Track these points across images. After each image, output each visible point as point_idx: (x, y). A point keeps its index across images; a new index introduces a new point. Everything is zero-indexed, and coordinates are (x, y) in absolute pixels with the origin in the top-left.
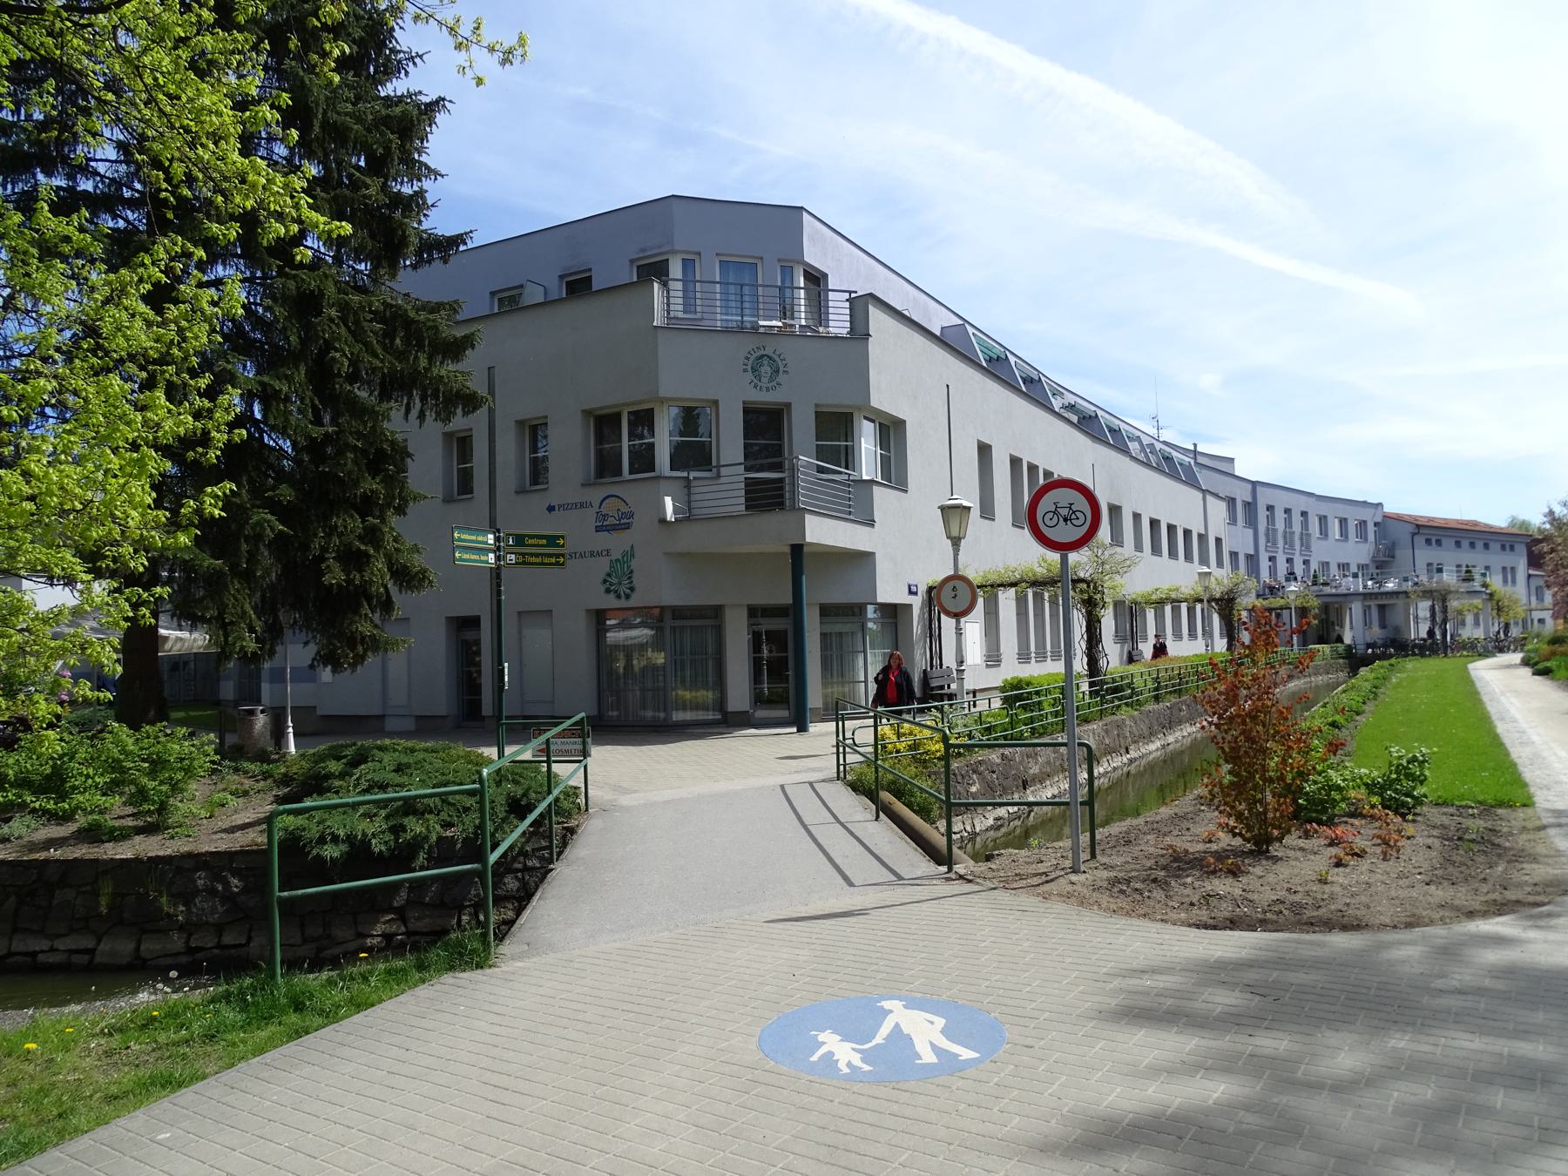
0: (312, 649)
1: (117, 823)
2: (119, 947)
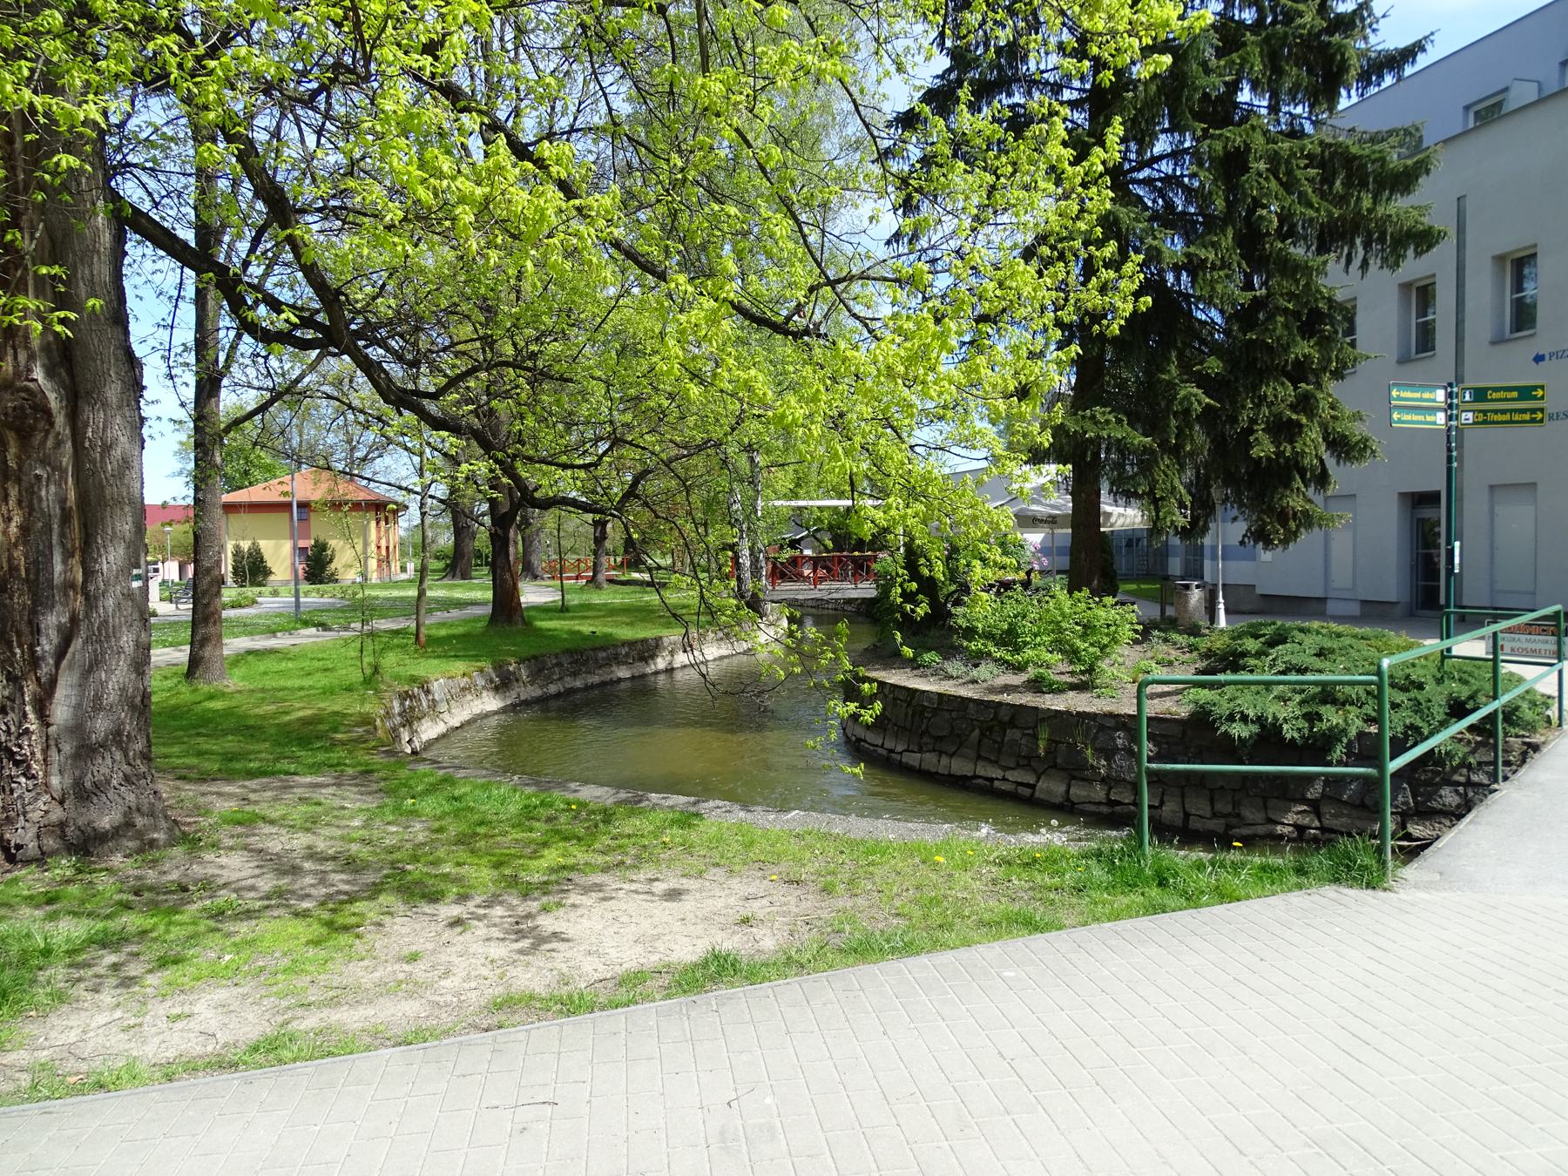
0: (1241, 527)
1: (1058, 678)
2: (1051, 787)
